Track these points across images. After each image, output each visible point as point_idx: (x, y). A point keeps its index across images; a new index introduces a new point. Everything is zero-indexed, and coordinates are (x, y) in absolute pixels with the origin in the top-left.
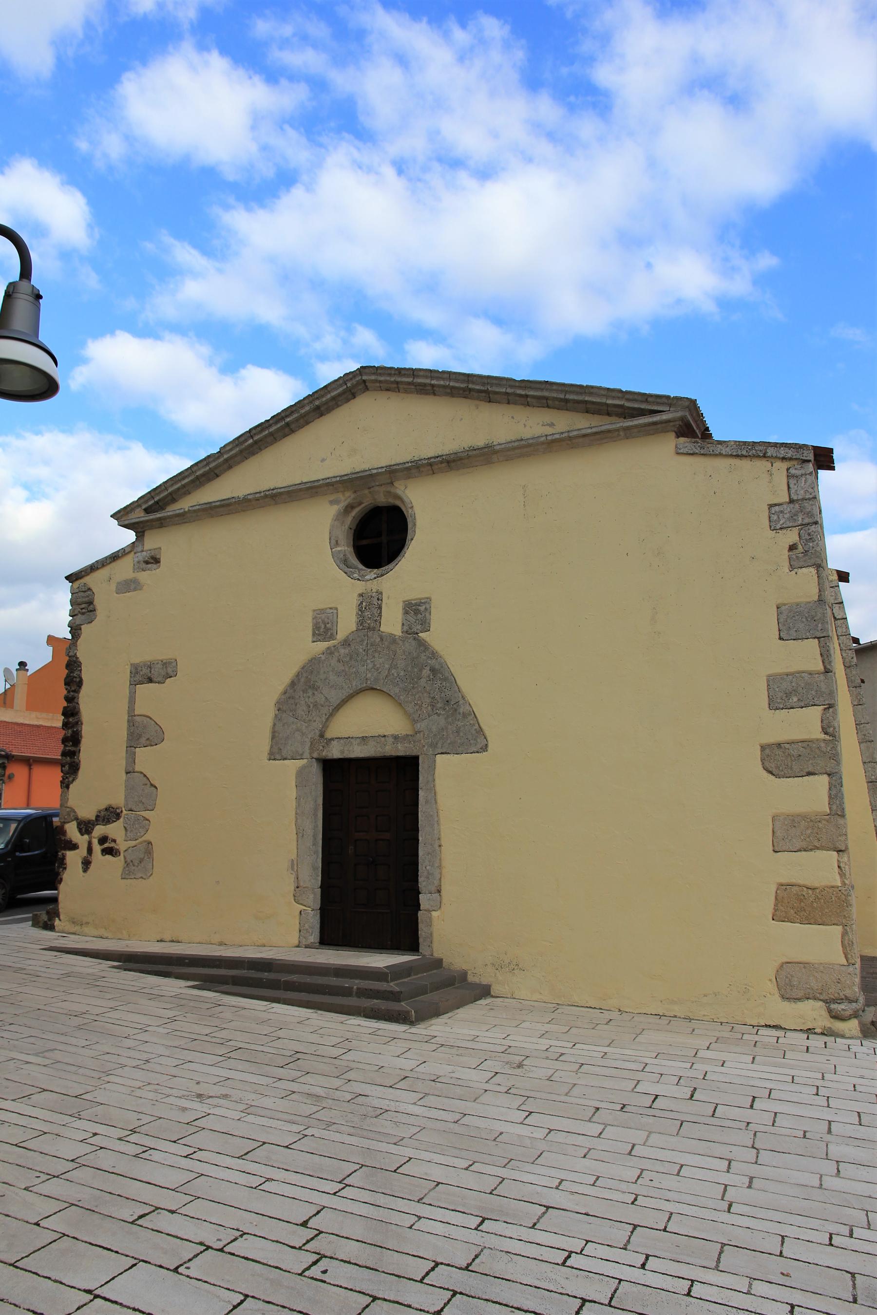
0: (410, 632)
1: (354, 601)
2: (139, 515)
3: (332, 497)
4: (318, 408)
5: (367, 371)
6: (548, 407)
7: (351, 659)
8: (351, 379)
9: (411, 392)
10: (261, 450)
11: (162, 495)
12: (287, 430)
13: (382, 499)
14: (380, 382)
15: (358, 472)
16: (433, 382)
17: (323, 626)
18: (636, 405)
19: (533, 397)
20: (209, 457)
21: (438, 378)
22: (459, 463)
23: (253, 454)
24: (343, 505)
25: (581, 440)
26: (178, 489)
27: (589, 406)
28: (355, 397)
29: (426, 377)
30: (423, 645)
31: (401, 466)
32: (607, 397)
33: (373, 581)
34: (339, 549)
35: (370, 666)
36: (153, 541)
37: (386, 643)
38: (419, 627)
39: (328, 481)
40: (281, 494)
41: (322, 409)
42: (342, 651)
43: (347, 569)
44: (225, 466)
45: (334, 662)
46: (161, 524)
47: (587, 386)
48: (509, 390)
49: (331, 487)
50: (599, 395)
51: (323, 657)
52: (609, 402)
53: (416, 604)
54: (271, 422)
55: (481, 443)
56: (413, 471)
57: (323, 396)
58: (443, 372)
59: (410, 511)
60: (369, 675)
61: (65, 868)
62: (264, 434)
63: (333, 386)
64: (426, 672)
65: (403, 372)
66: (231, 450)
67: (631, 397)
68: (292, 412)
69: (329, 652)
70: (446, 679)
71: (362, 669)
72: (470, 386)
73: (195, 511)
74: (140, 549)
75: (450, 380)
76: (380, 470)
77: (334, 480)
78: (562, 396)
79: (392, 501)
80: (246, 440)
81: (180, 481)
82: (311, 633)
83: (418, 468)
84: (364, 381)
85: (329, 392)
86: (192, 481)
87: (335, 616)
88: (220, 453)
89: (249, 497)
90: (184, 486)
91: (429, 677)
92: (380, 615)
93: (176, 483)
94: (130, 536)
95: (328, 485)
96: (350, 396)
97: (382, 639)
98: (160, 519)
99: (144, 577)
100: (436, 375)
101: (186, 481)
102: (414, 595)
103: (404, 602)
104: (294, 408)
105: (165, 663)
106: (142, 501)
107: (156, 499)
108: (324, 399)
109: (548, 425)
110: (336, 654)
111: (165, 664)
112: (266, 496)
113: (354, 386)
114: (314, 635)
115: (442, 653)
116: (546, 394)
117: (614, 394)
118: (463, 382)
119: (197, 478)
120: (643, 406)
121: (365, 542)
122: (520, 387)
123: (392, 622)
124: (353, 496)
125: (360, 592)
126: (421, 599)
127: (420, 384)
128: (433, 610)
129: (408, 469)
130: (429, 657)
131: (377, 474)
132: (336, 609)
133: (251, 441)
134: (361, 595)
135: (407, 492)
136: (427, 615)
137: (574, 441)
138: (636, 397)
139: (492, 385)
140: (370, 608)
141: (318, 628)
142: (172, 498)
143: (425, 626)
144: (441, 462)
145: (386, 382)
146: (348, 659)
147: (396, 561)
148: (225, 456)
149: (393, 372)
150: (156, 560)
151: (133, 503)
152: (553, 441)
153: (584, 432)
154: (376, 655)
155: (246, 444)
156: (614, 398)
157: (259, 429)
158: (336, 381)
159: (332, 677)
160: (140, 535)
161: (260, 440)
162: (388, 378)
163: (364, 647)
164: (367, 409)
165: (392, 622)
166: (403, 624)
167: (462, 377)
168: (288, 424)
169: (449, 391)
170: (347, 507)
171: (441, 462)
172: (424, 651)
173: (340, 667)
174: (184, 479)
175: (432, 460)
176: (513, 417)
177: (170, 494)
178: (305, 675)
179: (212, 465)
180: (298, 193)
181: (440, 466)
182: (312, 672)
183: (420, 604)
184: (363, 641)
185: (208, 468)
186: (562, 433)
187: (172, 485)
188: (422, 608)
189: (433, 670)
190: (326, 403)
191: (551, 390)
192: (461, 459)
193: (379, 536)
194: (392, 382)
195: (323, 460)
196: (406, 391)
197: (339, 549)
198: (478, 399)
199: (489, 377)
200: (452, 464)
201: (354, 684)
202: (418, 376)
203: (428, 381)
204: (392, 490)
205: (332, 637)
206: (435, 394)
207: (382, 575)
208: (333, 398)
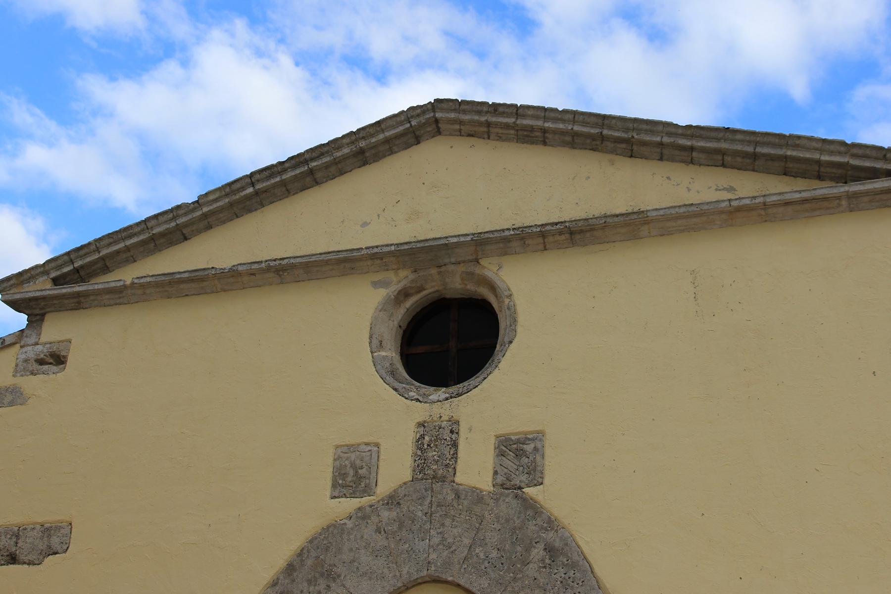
0: (507, 486)
1: (410, 434)
2: (43, 287)
3: (377, 277)
4: (362, 152)
5: (444, 105)
6: (723, 165)
7: (400, 528)
8: (418, 115)
9: (507, 140)
10: (262, 205)
11: (88, 259)
12: (308, 179)
13: (456, 284)
14: (461, 123)
15: (427, 240)
16: (546, 125)
17: (352, 473)
18: (868, 164)
19: (703, 150)
20: (178, 207)
21: (556, 120)
22: (588, 235)
23: (250, 211)
24: (394, 288)
25: (781, 209)
26: (118, 252)
27: (790, 165)
28: (418, 143)
29: (537, 118)
30: (532, 508)
31: (496, 235)
32: (821, 151)
33: (437, 404)
34: (384, 354)
35: (436, 540)
36: (54, 330)
37: (466, 503)
38: (524, 478)
39: (376, 250)
40: (293, 267)
41: (367, 154)
42: (385, 514)
44: (202, 225)
45: (368, 532)
46: (78, 303)
47: (791, 136)
48: (666, 140)
49: (379, 261)
50: (808, 149)
51: (350, 524)
52: (825, 158)
53: (518, 441)
54: (287, 165)
55: (621, 208)
57: (372, 136)
58: (565, 111)
59: (507, 301)
60: (433, 556)
62: (273, 181)
63: (390, 123)
64: (538, 552)
65: (501, 109)
66: (216, 200)
67: (860, 152)
68: (322, 154)
69: (362, 515)
70: (574, 566)
71: (421, 545)
72: (605, 132)
73: (142, 286)
74: (33, 340)
75: (574, 122)
76: (462, 239)
78: (750, 149)
80: (243, 188)
81: (123, 239)
82: (329, 483)
83: (522, 239)
84: (437, 121)
85: (383, 131)
86: (143, 243)
87: (374, 455)
88: (198, 203)
89: (240, 268)
90: (128, 249)
91: (543, 560)
92: (455, 456)
93: (116, 242)
94: (20, 320)
96: (413, 140)
97: (458, 496)
98: (78, 295)
99: (31, 384)
100: (552, 115)
101: (135, 240)
102: (514, 426)
103: (497, 437)
104: (326, 149)
105: (47, 529)
106: (53, 265)
107: (76, 265)
108: (374, 140)
109: (724, 189)
110: (374, 519)
111: (47, 531)
112: (269, 269)
113: (421, 126)
114: (334, 485)
115: (565, 522)
116: (724, 145)
117: (832, 147)
118: (596, 125)
119: (153, 238)
120: (879, 165)
121: (420, 349)
122: (684, 136)
123: (476, 468)
124: (412, 276)
125: (420, 419)
126: (526, 433)
127: (525, 128)
128: (548, 451)
129: (506, 240)
130: (542, 528)
131: (458, 245)
132: (377, 445)
133: (250, 190)
134: (421, 425)
135: (501, 273)
136: (538, 458)
137: (770, 211)
138: (868, 152)
139: (639, 131)
140: (436, 448)
141: (344, 476)
142: (104, 266)
143: (536, 476)
144: (561, 233)
145: (471, 122)
146: (395, 527)
147: (472, 382)
148: (205, 209)
149: (485, 109)
150: (58, 360)
151: (37, 267)
152: (739, 209)
153: (788, 197)
154: (448, 522)
155: (244, 193)
156: (832, 153)
157: (266, 173)
158: (394, 116)
159: (365, 558)
160: (36, 320)
161: (265, 191)
162: (476, 118)
163: (425, 508)
164: (434, 156)
165: (476, 468)
166: (496, 473)
167: (593, 120)
168: (311, 172)
169: (568, 139)
170: (400, 292)
171: (561, 233)
172: (534, 518)
173: (381, 541)
174: (130, 237)
175: (548, 228)
176: (668, 178)
177: (103, 259)
178: (313, 554)
179: (181, 221)
180: (171, 68)
181: (558, 238)
182: (327, 549)
183: (525, 441)
184: (423, 498)
185: (173, 224)
186: (754, 198)
187: (109, 245)
188: (529, 448)
189: (550, 549)
190: (375, 146)
191: (733, 141)
192: (592, 229)
193: (449, 336)
194: (480, 124)
195: (365, 224)
196: (500, 138)
197: (384, 354)
198: (613, 152)
199: (636, 120)
200: (577, 237)
201: (405, 571)
202: (524, 116)
203: (539, 123)
204: (478, 271)
205: (368, 491)
206: (545, 143)
207: (459, 395)
208: (387, 141)
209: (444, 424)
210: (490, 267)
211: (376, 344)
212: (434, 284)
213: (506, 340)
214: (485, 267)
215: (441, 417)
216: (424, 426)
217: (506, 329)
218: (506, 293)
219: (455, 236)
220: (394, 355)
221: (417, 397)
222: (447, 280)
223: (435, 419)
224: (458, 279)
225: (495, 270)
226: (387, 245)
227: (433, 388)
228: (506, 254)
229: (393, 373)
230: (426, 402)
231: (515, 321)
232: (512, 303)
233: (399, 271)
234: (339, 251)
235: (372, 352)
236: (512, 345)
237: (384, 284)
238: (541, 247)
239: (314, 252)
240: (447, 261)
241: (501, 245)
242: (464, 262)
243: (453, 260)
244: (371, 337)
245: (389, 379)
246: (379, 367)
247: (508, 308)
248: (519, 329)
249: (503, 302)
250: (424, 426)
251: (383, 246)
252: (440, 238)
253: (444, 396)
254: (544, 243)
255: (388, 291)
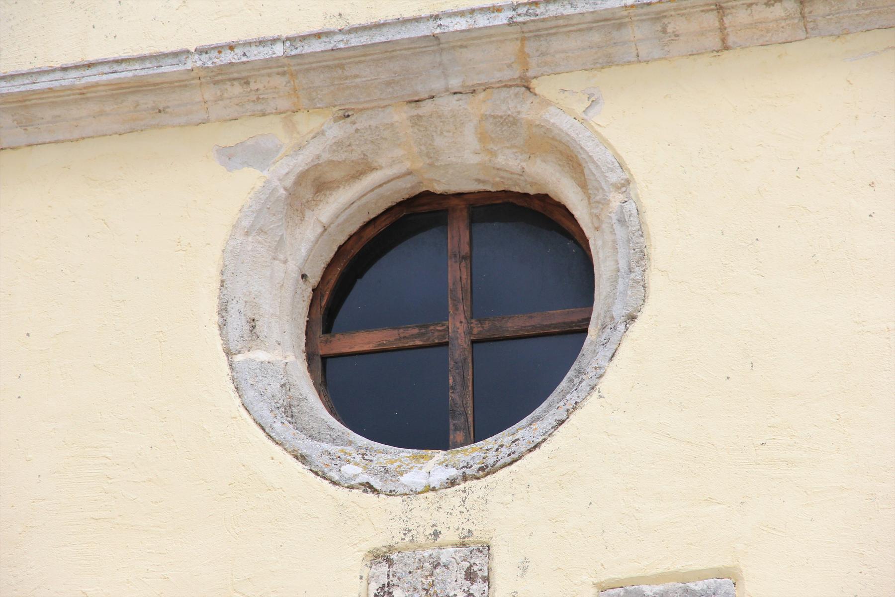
13: (465, 159)
15: (378, 26)
24: (286, 167)
34: (261, 356)
39: (228, 57)
43: (305, 445)
49: (237, 89)
56: (637, 32)
59: (616, 199)
61: (649, 260)
76: (482, 21)
77: (258, 54)
79: (333, 330)
95: (221, 76)
125: (379, 542)
131: (468, 38)
134: (383, 557)
147: (522, 432)
197: (261, 356)
204: (527, 111)
207: (486, 470)
209: (446, 555)
210: (566, 104)
211: (240, 330)
212: (399, 152)
213: (619, 311)
214: (547, 103)
215: (436, 534)
216: (388, 560)
217: (614, 282)
218: (615, 177)
219: (462, 14)
220: (291, 358)
221: (364, 478)
222: (440, 142)
223: (421, 539)
224: (470, 138)
225: (579, 108)
226: (261, 42)
227: (406, 454)
228: (609, 62)
229: (290, 411)
230: (391, 493)
231: (643, 256)
232: (631, 206)
233: (298, 117)
234: (119, 62)
235: (228, 353)
236: (635, 327)
237: (257, 155)
238: (714, 41)
239: (39, 64)
240: (437, 85)
241: (596, 37)
242: (487, 88)
243: (455, 83)
244: (223, 309)
245: (282, 428)
246: (250, 394)
247: (622, 221)
248: (655, 280)
249: (606, 202)
250: (388, 560)
251: (249, 44)
252: (417, 20)
253: (442, 475)
254: (722, 28)
255: (266, 173)
